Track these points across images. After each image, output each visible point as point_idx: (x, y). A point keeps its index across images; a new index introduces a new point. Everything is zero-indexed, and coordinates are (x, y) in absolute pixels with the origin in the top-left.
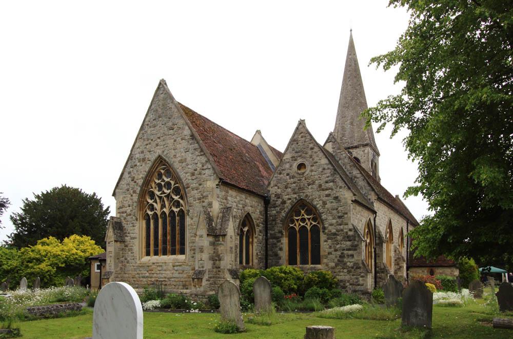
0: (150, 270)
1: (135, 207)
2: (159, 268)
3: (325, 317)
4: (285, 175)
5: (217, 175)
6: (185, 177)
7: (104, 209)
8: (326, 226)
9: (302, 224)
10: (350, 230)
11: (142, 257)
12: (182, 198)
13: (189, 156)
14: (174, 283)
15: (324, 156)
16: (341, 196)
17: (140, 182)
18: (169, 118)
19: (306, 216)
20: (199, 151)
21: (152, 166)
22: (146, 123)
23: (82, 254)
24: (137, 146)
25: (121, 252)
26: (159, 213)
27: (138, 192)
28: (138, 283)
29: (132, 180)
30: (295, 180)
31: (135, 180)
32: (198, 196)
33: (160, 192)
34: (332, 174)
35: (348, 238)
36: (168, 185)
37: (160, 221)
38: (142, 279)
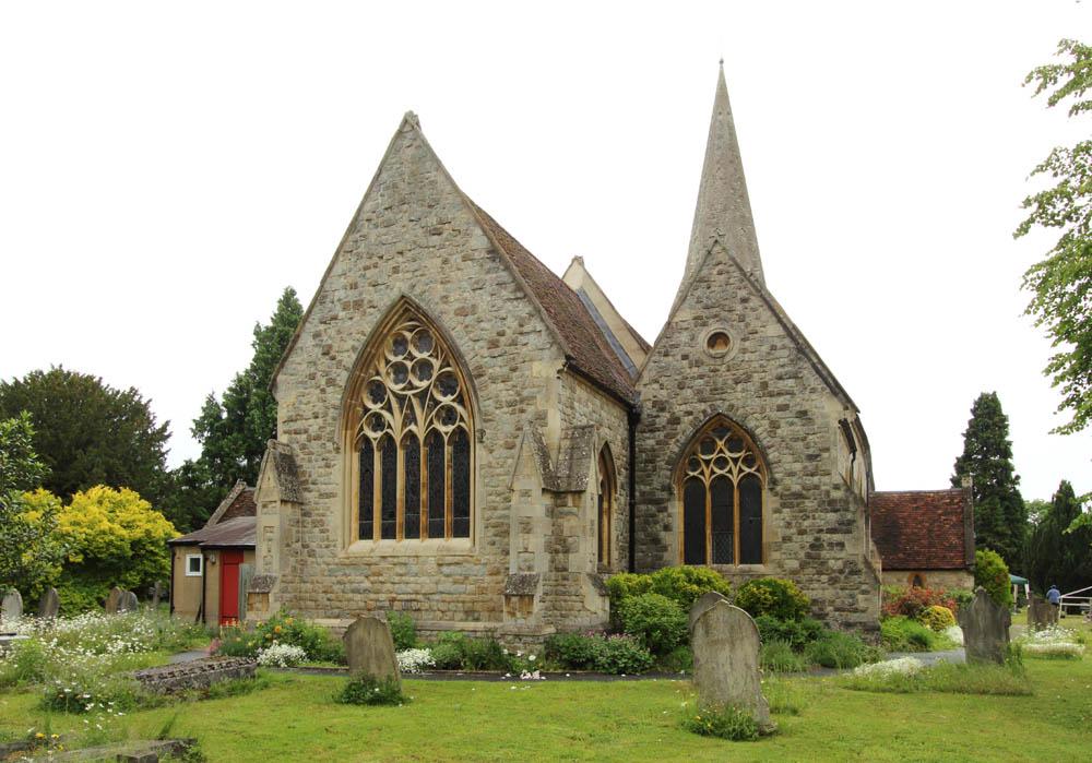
0: (374, 574)
1: (334, 419)
2: (398, 569)
3: (866, 689)
4: (679, 357)
5: (560, 348)
6: (473, 351)
7: (158, 426)
8: (777, 476)
9: (719, 472)
10: (836, 487)
11: (350, 543)
12: (460, 400)
13: (483, 301)
14: (443, 607)
15: (774, 318)
16: (814, 409)
17: (349, 359)
18: (430, 206)
19: (728, 454)
20: (510, 290)
21: (382, 322)
22: (365, 216)
23: (124, 532)
24: (338, 269)
25: (294, 529)
26: (398, 437)
27: (343, 384)
28: (338, 604)
29: (324, 354)
30: (704, 370)
31: (332, 353)
32: (505, 396)
33: (402, 386)
34: (792, 361)
35: (832, 506)
36: (424, 368)
37: (401, 455)
38: (350, 595)
